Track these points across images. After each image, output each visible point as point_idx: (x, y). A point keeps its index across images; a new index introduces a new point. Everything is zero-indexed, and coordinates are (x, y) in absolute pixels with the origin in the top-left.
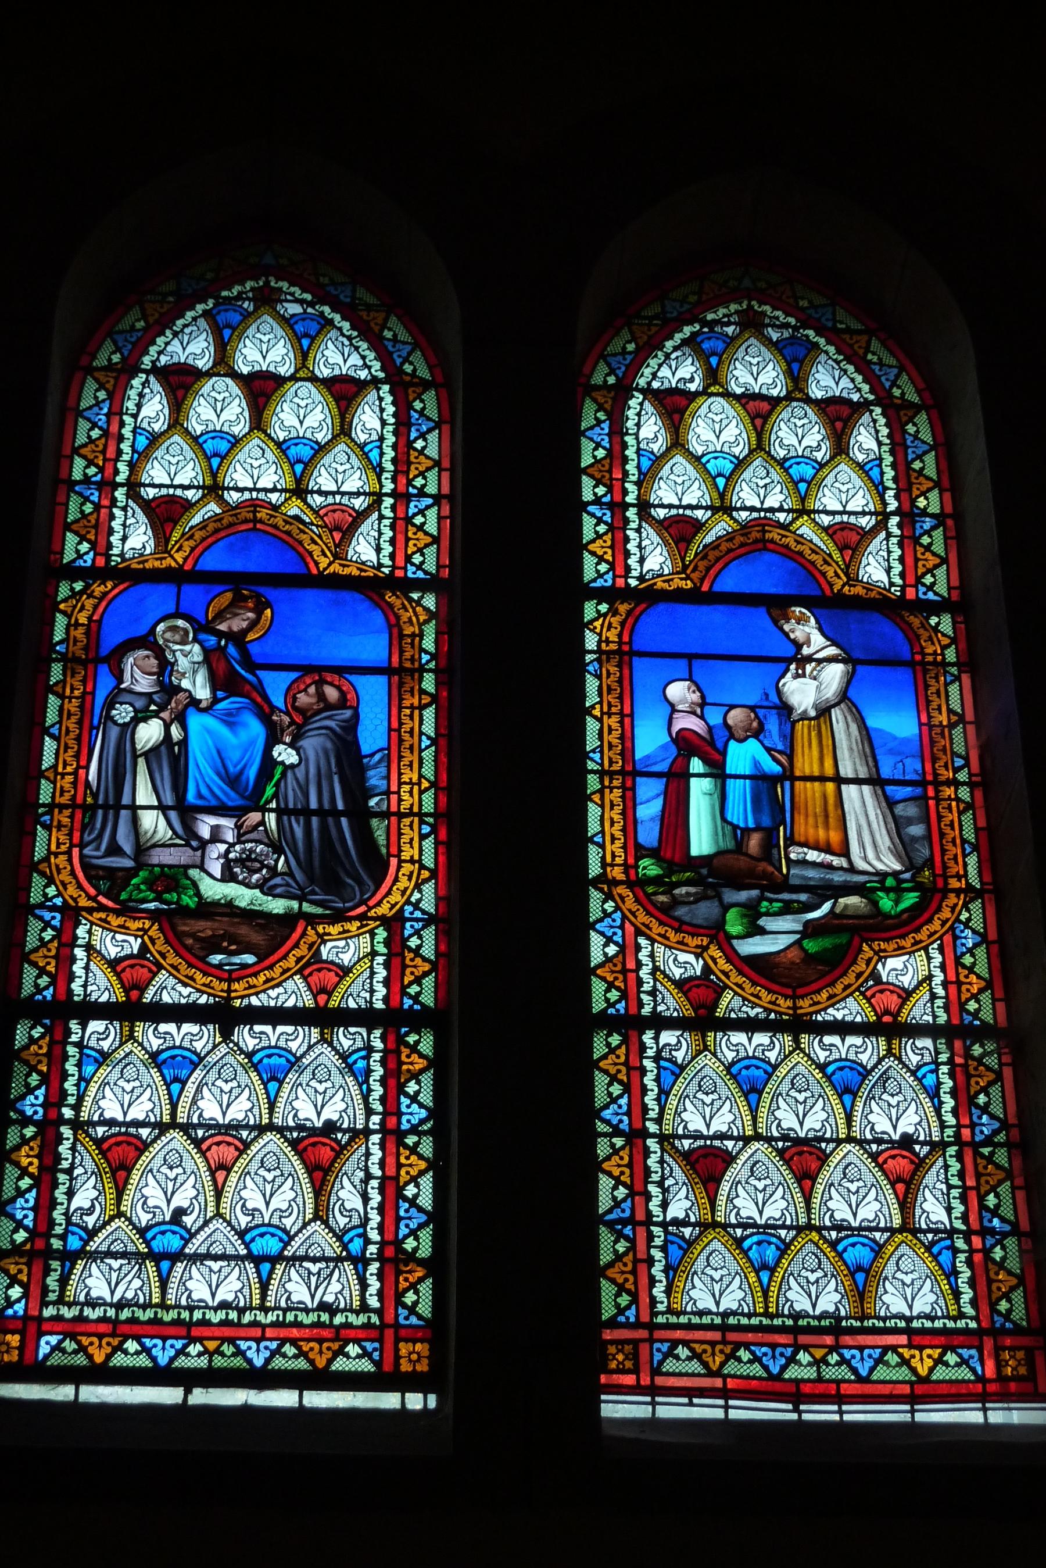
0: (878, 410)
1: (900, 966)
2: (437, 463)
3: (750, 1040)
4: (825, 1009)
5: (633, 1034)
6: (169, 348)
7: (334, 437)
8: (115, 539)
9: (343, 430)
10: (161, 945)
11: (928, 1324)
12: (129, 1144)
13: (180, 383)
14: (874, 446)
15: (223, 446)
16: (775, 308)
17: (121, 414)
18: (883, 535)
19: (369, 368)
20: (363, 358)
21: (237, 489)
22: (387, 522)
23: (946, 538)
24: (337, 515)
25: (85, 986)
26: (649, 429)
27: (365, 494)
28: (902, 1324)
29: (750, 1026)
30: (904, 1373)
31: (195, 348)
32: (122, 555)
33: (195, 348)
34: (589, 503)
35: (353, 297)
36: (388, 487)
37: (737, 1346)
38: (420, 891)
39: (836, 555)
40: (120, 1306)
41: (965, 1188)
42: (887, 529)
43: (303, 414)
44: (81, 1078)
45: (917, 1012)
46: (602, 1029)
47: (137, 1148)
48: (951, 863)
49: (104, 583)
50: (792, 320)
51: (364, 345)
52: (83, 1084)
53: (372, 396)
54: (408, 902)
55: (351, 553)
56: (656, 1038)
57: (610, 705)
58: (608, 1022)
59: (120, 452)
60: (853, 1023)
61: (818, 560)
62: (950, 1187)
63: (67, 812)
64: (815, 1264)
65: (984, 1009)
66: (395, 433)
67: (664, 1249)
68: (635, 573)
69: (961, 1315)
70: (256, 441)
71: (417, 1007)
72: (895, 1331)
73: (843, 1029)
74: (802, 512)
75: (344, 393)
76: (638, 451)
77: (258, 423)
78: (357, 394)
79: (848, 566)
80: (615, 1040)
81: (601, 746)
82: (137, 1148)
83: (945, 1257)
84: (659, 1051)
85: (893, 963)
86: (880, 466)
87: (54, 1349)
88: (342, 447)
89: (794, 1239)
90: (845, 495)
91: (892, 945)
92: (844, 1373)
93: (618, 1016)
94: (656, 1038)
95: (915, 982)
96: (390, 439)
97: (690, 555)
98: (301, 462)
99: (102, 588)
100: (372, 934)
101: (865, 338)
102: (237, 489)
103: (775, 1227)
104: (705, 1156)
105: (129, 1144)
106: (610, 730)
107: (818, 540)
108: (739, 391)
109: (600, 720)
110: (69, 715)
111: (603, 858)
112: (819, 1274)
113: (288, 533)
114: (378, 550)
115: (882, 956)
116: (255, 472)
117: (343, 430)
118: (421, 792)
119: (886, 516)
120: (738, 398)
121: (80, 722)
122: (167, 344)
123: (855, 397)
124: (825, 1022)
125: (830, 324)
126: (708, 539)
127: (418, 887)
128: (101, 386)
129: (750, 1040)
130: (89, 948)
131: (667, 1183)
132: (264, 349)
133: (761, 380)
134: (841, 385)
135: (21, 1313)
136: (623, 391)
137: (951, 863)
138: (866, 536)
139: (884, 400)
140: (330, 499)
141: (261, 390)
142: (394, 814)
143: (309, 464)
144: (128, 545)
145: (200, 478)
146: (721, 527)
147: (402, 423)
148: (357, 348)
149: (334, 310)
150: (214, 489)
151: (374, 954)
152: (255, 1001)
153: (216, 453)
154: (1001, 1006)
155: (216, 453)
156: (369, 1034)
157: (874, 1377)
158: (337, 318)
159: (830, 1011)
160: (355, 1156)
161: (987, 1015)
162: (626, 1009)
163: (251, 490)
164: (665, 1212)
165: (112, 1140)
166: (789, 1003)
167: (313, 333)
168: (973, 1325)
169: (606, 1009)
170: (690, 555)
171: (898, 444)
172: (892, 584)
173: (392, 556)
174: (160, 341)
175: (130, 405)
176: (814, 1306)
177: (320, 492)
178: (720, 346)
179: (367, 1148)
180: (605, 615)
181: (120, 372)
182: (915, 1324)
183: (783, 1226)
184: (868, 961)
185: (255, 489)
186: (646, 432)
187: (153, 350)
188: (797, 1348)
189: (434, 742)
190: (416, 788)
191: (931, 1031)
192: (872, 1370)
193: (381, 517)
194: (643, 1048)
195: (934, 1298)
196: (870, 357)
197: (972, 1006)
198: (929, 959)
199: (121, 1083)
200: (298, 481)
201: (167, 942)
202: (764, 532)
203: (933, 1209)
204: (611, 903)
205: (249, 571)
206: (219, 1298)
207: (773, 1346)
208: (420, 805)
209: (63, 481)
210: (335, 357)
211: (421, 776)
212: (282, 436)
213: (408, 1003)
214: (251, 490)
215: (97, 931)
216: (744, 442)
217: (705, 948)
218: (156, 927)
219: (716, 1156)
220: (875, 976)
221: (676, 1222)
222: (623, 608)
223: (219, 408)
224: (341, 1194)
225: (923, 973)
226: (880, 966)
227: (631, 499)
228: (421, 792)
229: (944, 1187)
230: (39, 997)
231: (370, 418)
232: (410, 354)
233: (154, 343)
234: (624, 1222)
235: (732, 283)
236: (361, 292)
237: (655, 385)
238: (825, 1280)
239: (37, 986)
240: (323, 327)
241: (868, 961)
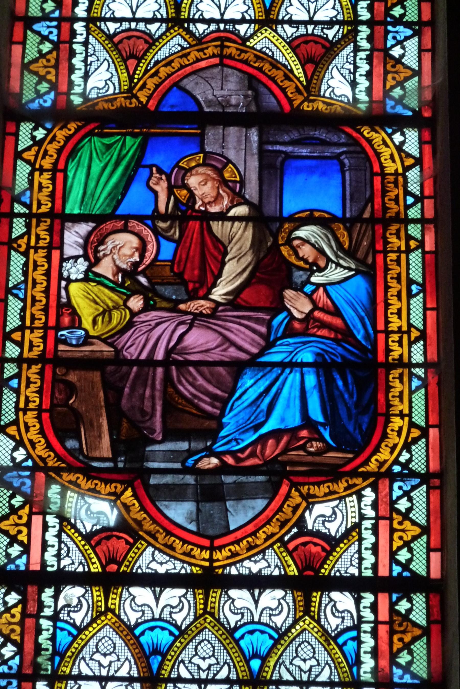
1: (328, 512)
3: (157, 600)
4: (242, 561)
8: (77, 77)
18: (351, 47)
22: (362, 55)
23: (421, 50)
25: (58, 556)
32: (83, 95)
39: (298, 71)
42: (355, 42)
44: (55, 652)
48: (396, 402)
52: (57, 659)
54: (396, 462)
55: (324, 87)
56: (56, 597)
57: (38, 238)
61: (279, 75)
63: (35, 368)
65: (421, 560)
71: (406, 574)
73: (257, 583)
79: (309, 81)
91: (324, 489)
93: (17, 572)
94: (56, 597)
95: (343, 530)
99: (65, 132)
106: (36, 266)
107: (285, 56)
109: (26, 254)
110: (36, 266)
111: (17, 403)
113: (260, 69)
114: (354, 84)
124: (240, 576)
126: (161, 55)
127: (407, 447)
130: (63, 519)
137: (396, 402)
138: (331, 49)
142: (49, 361)
144: (91, 83)
145: (163, 11)
152: (234, 571)
154: (436, 557)
156: (358, 601)
159: (247, 563)
161: (419, 567)
162: (28, 564)
163: (129, 20)
169: (6, 565)
173: (369, 91)
184: (296, 508)
185: (222, 21)
189: (423, 288)
190: (405, 337)
193: (357, 49)
197: (403, 555)
199: (196, 660)
202: (222, 47)
208: (410, 357)
209: (20, 19)
214: (129, 20)
215: (71, 496)
217: (118, 496)
226: (307, 514)
230: (11, 567)
241: (296, 508)
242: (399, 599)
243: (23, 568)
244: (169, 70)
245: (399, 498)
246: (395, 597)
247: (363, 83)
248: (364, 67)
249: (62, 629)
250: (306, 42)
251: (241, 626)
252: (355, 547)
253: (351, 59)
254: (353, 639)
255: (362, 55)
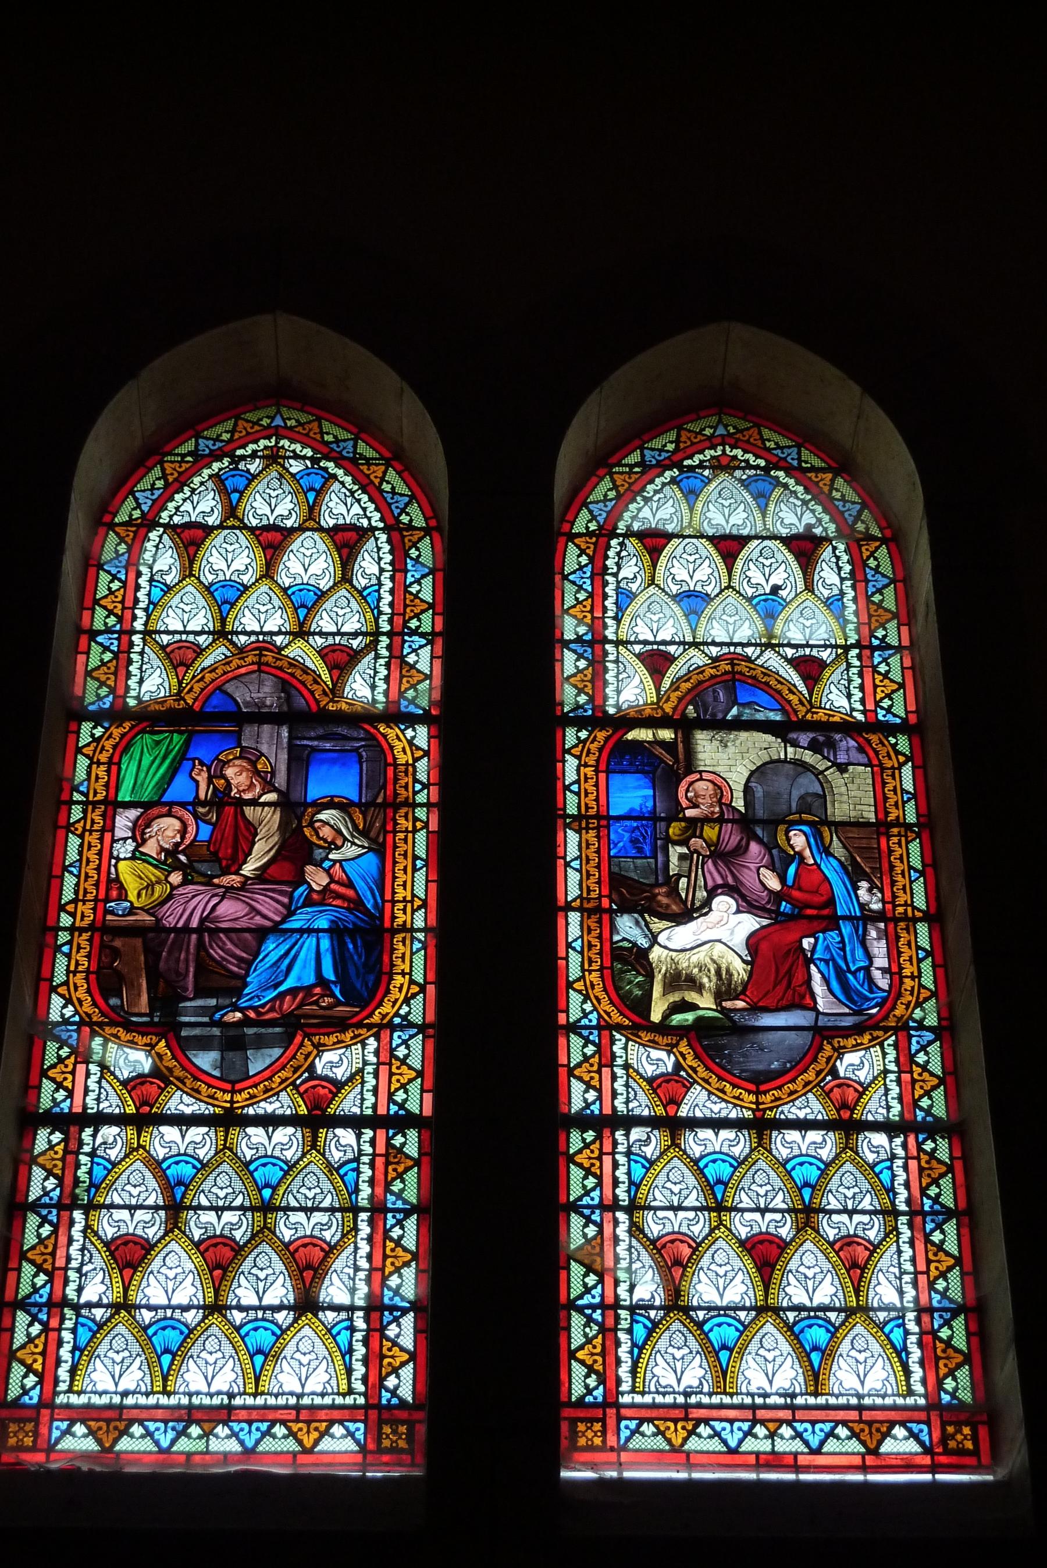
0: (383, 537)
1: (336, 1059)
2: (431, 606)
3: (803, 1137)
5: (606, 1133)
6: (641, 515)
7: (335, 584)
9: (346, 578)
10: (691, 1061)
11: (879, 1401)
12: (225, 1245)
13: (191, 539)
14: (836, 580)
15: (231, 594)
16: (745, 451)
17: (137, 564)
19: (369, 519)
20: (364, 509)
21: (245, 633)
22: (382, 661)
24: (335, 655)
26: (161, 557)
27: (362, 634)
28: (854, 1401)
29: (717, 1124)
30: (715, 1445)
31: (202, 505)
32: (137, 698)
33: (202, 505)
34: (571, 641)
35: (355, 452)
36: (385, 627)
37: (698, 1422)
38: (409, 1005)
40: (687, 1394)
41: (916, 1273)
42: (376, 650)
43: (309, 562)
45: (872, 1106)
46: (44, 1125)
47: (779, 1246)
49: (120, 725)
50: (762, 463)
51: (365, 498)
53: (370, 544)
54: (397, 1014)
56: (627, 1135)
58: (583, 1122)
59: (136, 601)
60: (283, 1116)
62: (357, 1269)
63: (85, 936)
64: (681, 1342)
66: (392, 579)
67: (74, 1331)
68: (133, 693)
69: (350, 1391)
70: (344, 592)
71: (929, 1119)
72: (847, 1407)
73: (803, 1125)
74: (302, 632)
75: (347, 542)
76: (151, 580)
77: (268, 572)
78: (360, 539)
80: (57, 1137)
81: (80, 860)
82: (779, 1246)
83: (343, 1338)
84: (629, 1147)
85: (329, 1056)
86: (378, 591)
87: (633, 1433)
88: (264, 588)
89: (662, 1318)
90: (808, 626)
91: (851, 1041)
92: (798, 1446)
95: (870, 1077)
96: (388, 585)
97: (666, 683)
98: (305, 606)
99: (121, 730)
100: (364, 1045)
101: (830, 476)
102: (245, 633)
103: (736, 1309)
104: (126, 1243)
105: (315, 1245)
108: (254, 522)
109: (81, 836)
110: (90, 847)
112: (686, 1351)
115: (320, 1049)
116: (261, 616)
117: (346, 578)
118: (413, 911)
119: (377, 634)
120: (252, 530)
121: (100, 853)
122: (639, 510)
123: (365, 523)
125: (795, 463)
126: (207, 663)
128: (122, 540)
129: (803, 1137)
130: (103, 1067)
131: (85, 1269)
132: (271, 503)
133: (732, 521)
134: (353, 512)
135: (600, 1399)
136: (606, 533)
138: (354, 657)
139: (394, 528)
140: (253, 638)
141: (273, 541)
143: (312, 609)
144: (145, 687)
145: (211, 625)
146: (219, 653)
147: (399, 567)
148: (359, 501)
149: (338, 466)
150: (221, 633)
151: (886, 1072)
153: (225, 598)
155: (225, 598)
157: (743, 1449)
158: (340, 472)
159: (262, 1104)
160: (888, 1254)
164: (79, 1297)
165: (299, 1242)
166: (752, 1098)
167: (241, 488)
168: (922, 1401)
170: (666, 683)
171: (858, 576)
172: (852, 710)
174: (633, 507)
175: (148, 556)
176: (679, 1381)
177: (321, 634)
178: (241, 482)
179: (898, 1246)
180: (584, 742)
181: (138, 526)
182: (867, 1401)
183: (743, 1308)
185: (261, 633)
186: (161, 565)
187: (627, 515)
188: (755, 1422)
190: (409, 905)
191: (888, 1128)
192: (741, 1442)
193: (377, 657)
194: (81, 1143)
195: (233, 1376)
196: (834, 493)
198: (884, 1054)
200: (301, 625)
201: (696, 1056)
203: (884, 1291)
204: (71, 1008)
205: (260, 708)
206: (684, 1383)
207: (813, 1423)
209: (85, 632)
210: (341, 507)
211: (413, 895)
212: (287, 582)
213: (394, 1109)
214: (180, 633)
216: (726, 578)
218: (163, 1043)
219: (771, 1242)
220: (834, 1072)
221: (90, 1305)
222: (601, 735)
223: (230, 558)
224: (698, 1287)
225: (878, 1068)
226: (838, 1063)
227: (138, 625)
228: (413, 911)
229: (896, 1271)
230: (57, 1110)
231: (372, 563)
232: (407, 505)
233: (172, 499)
234: (593, 1307)
235: (708, 432)
236: (362, 448)
237: (176, 519)
238: (690, 1357)
239: (54, 1100)
240: (327, 480)
241: (829, 1059)
242: (925, 1140)
243: (597, 1112)
244: (213, 675)
245: (398, 1046)
246: (391, 1132)
247: (857, 695)
248: (383, 672)
249: (98, 1164)
250: (334, 651)
251: (878, 1163)
252: (882, 1091)
253: (372, 666)
254: (353, 1170)
255: (382, 661)
